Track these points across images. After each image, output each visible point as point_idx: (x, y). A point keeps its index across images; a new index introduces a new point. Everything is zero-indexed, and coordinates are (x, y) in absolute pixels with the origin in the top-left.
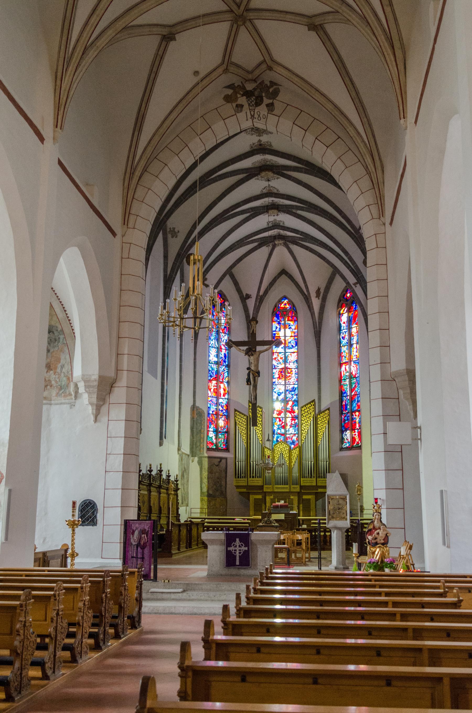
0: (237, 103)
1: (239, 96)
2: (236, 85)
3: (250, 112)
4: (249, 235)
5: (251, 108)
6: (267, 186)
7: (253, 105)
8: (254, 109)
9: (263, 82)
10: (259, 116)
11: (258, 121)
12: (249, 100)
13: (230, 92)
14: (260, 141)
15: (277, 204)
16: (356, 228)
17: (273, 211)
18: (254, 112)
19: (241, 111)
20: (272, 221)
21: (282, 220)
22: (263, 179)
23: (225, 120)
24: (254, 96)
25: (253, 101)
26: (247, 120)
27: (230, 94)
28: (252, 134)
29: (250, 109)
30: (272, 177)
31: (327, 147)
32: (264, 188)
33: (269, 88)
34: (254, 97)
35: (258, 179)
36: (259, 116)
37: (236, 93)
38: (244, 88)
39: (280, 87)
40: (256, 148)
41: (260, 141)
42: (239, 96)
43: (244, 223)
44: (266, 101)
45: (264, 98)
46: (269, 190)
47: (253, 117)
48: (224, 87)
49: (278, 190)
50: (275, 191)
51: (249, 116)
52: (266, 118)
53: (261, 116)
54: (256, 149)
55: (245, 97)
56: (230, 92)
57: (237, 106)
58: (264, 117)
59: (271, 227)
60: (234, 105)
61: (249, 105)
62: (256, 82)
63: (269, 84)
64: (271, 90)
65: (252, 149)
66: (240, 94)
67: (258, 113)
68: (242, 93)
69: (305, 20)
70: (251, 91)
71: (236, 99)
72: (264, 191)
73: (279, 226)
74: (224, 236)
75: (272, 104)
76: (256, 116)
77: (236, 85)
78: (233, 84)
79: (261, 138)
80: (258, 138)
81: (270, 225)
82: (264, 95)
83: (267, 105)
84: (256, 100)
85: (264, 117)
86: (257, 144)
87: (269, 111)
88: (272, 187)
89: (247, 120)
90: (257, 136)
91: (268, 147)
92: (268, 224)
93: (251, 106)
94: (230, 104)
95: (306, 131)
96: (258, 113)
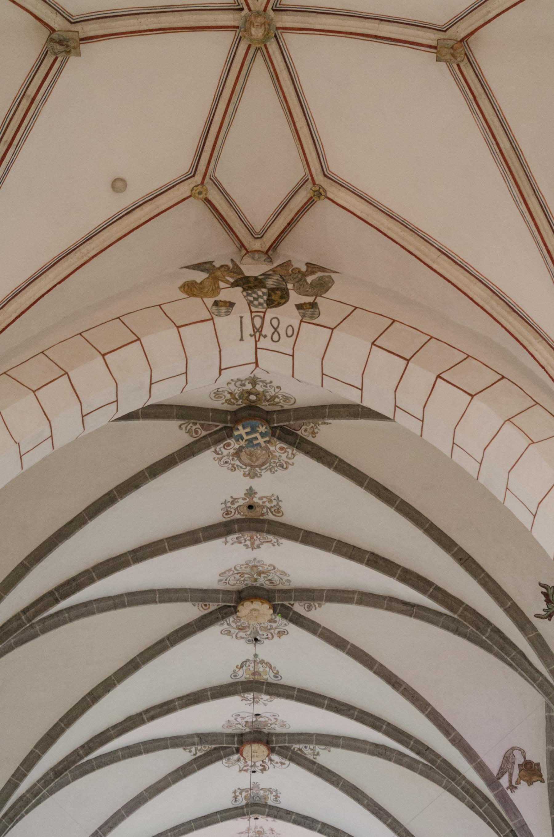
0: (218, 298)
1: (222, 285)
2: (217, 264)
3: (252, 319)
4: (183, 824)
5: (253, 309)
6: (251, 658)
7: (260, 304)
8: (265, 313)
9: (289, 263)
10: (276, 329)
11: (273, 346)
12: (248, 295)
13: (200, 276)
14: (251, 492)
15: (266, 731)
16: (491, 774)
17: (255, 747)
18: (263, 319)
19: (228, 313)
20: (246, 790)
21: (274, 788)
22: (241, 634)
23: (180, 329)
24: (265, 287)
25: (260, 297)
26: (242, 339)
27: (199, 281)
28: (234, 468)
29: (251, 312)
30: (266, 629)
31: (472, 396)
32: (242, 667)
33: (304, 275)
34: (264, 290)
35: (229, 633)
36: (276, 329)
37: (216, 280)
38: (237, 270)
39: (333, 276)
40: (237, 516)
41: (251, 492)
42: (222, 285)
43: (175, 781)
44: (295, 298)
45: (292, 294)
46: (254, 674)
47: (258, 332)
48: (188, 267)
49: (276, 675)
50: (269, 677)
51: (248, 329)
52: (295, 334)
53: (282, 330)
54: (238, 520)
55: (240, 289)
56: (200, 276)
57: (216, 303)
58: (290, 333)
59: (242, 808)
60: (210, 301)
61: (250, 303)
62: (271, 262)
63: (304, 269)
64: (309, 279)
65: (228, 518)
66: (227, 282)
67: (275, 323)
68: (232, 280)
69: (429, 37)
70: (256, 278)
71: (216, 290)
72: (240, 673)
73: (265, 805)
74: (116, 814)
75: (314, 305)
76: (267, 330)
77: (217, 264)
78: (211, 263)
79: (255, 484)
80: (248, 483)
81: (242, 802)
82: (290, 286)
83: (299, 307)
84: (269, 295)
85: (290, 332)
86: (241, 502)
87: (303, 316)
88: (262, 662)
89: (242, 339)
90: (244, 475)
91: (270, 517)
92: (236, 797)
93: (256, 306)
94: (198, 300)
95: (408, 361)
96: (275, 323)
